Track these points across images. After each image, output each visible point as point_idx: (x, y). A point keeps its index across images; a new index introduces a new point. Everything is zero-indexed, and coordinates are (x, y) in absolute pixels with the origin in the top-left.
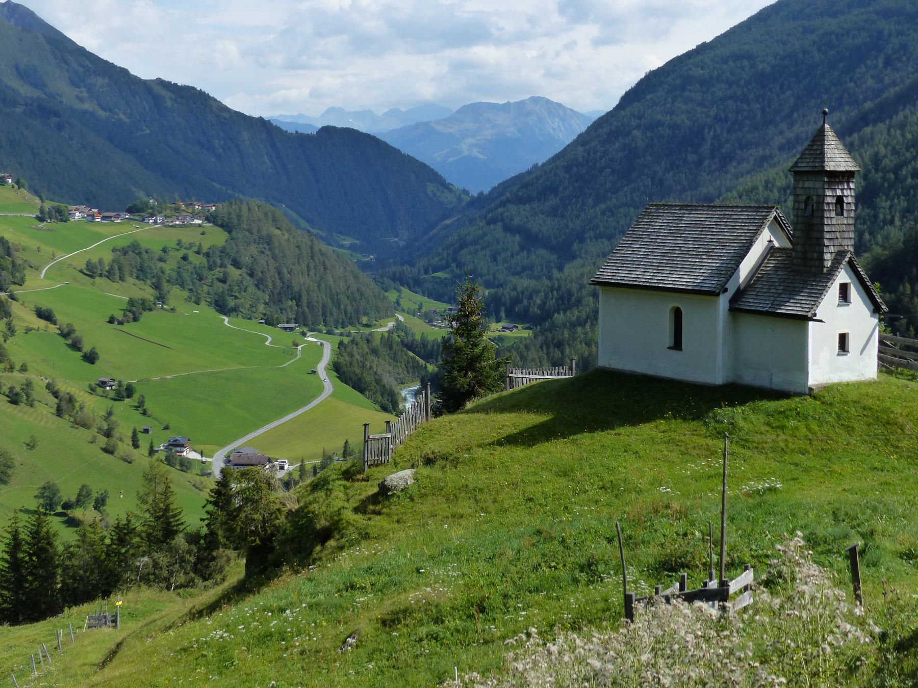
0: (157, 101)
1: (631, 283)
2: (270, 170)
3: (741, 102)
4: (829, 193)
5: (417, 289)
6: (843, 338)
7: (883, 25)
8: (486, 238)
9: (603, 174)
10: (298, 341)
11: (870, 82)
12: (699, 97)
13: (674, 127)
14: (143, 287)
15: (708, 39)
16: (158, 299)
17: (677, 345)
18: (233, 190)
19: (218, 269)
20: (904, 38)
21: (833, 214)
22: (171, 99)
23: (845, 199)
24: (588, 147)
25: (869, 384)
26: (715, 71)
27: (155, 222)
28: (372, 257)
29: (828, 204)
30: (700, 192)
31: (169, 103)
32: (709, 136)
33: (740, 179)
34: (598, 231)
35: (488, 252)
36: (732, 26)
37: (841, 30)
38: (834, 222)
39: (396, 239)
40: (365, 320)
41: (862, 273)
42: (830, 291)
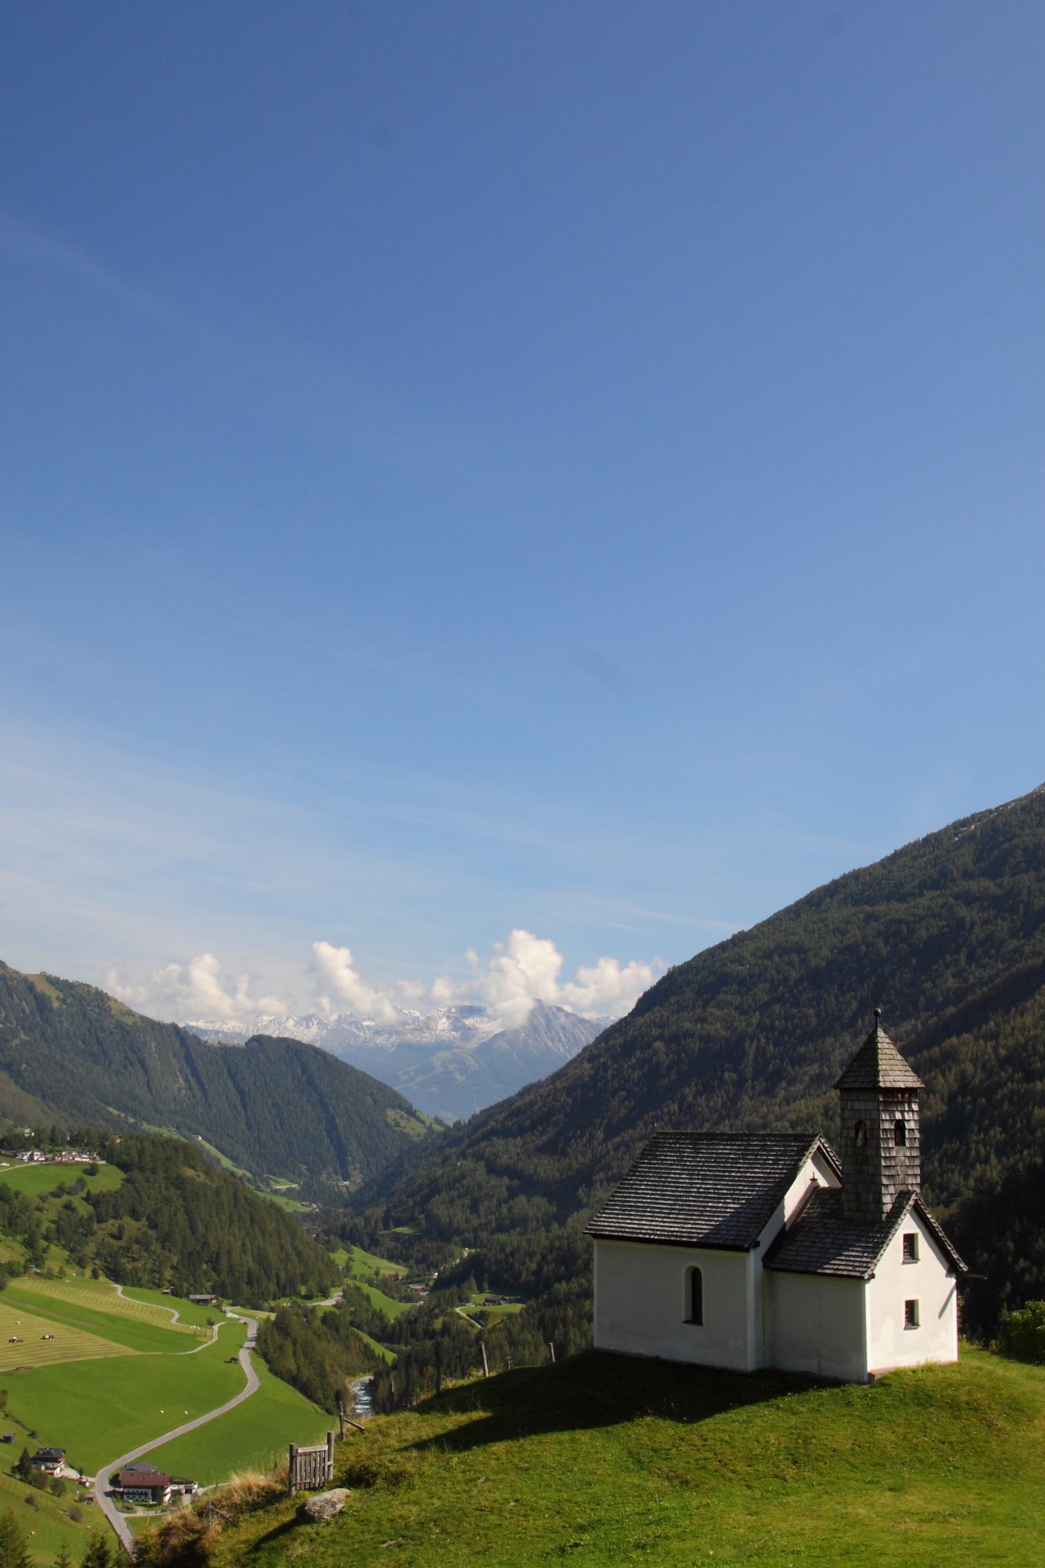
0: (41, 1003)
1: (634, 1235)
2: (184, 1092)
3: (791, 1007)
4: (885, 1116)
5: (373, 1249)
6: (911, 1307)
7: (962, 912)
8: (465, 1182)
9: (617, 1099)
10: (213, 1320)
11: (952, 982)
12: (737, 1000)
13: (707, 1039)
14: (11, 1244)
15: (747, 927)
16: (30, 1261)
17: (696, 1317)
18: (134, 1117)
19: (111, 1221)
20: (990, 927)
21: (891, 1144)
22: (58, 998)
23: (906, 1124)
24: (596, 1063)
25: (951, 1365)
26: (757, 968)
27: (31, 1158)
28: (314, 1206)
29: (885, 1130)
30: (742, 1122)
31: (56, 1004)
32: (751, 1049)
33: (792, 1105)
34: (610, 1173)
35: (467, 1202)
36: (776, 910)
37: (912, 918)
38: (894, 1154)
39: (347, 1183)
40: (303, 1290)
41: (932, 1220)
42: (891, 1244)
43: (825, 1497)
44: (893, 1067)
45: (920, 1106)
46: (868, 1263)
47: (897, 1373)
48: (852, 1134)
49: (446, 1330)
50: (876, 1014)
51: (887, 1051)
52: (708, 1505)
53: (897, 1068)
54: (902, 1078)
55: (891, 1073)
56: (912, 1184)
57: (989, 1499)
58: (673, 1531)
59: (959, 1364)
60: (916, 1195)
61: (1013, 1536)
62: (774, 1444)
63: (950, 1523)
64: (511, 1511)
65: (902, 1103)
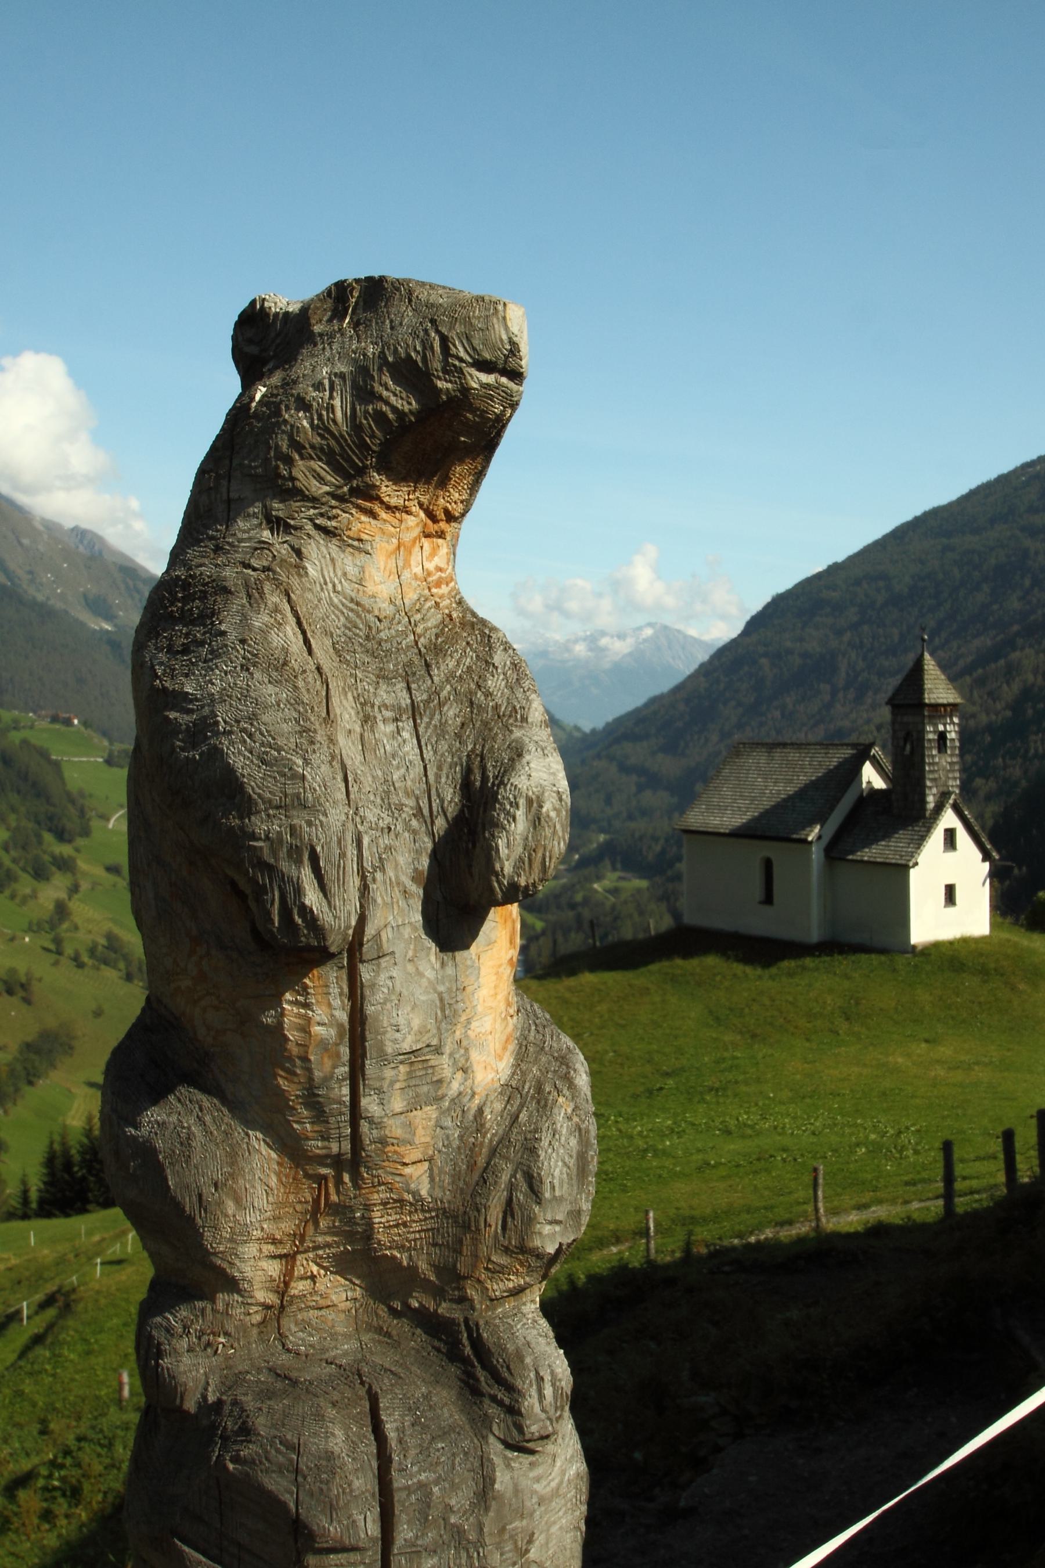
17: (768, 899)
21: (935, 752)
25: (982, 939)
29: (929, 740)
38: (937, 760)
43: (871, 1048)
44: (937, 686)
45: (960, 719)
46: (913, 852)
47: (937, 945)
48: (902, 743)
49: (586, 901)
50: (923, 640)
51: (932, 672)
52: (772, 1055)
53: (940, 687)
54: (945, 695)
55: (935, 691)
56: (952, 786)
57: (1009, 1050)
58: (741, 1078)
59: (989, 937)
60: (956, 794)
61: (1025, 1081)
62: (830, 1004)
63: (973, 1070)
64: (611, 1062)
65: (944, 717)
